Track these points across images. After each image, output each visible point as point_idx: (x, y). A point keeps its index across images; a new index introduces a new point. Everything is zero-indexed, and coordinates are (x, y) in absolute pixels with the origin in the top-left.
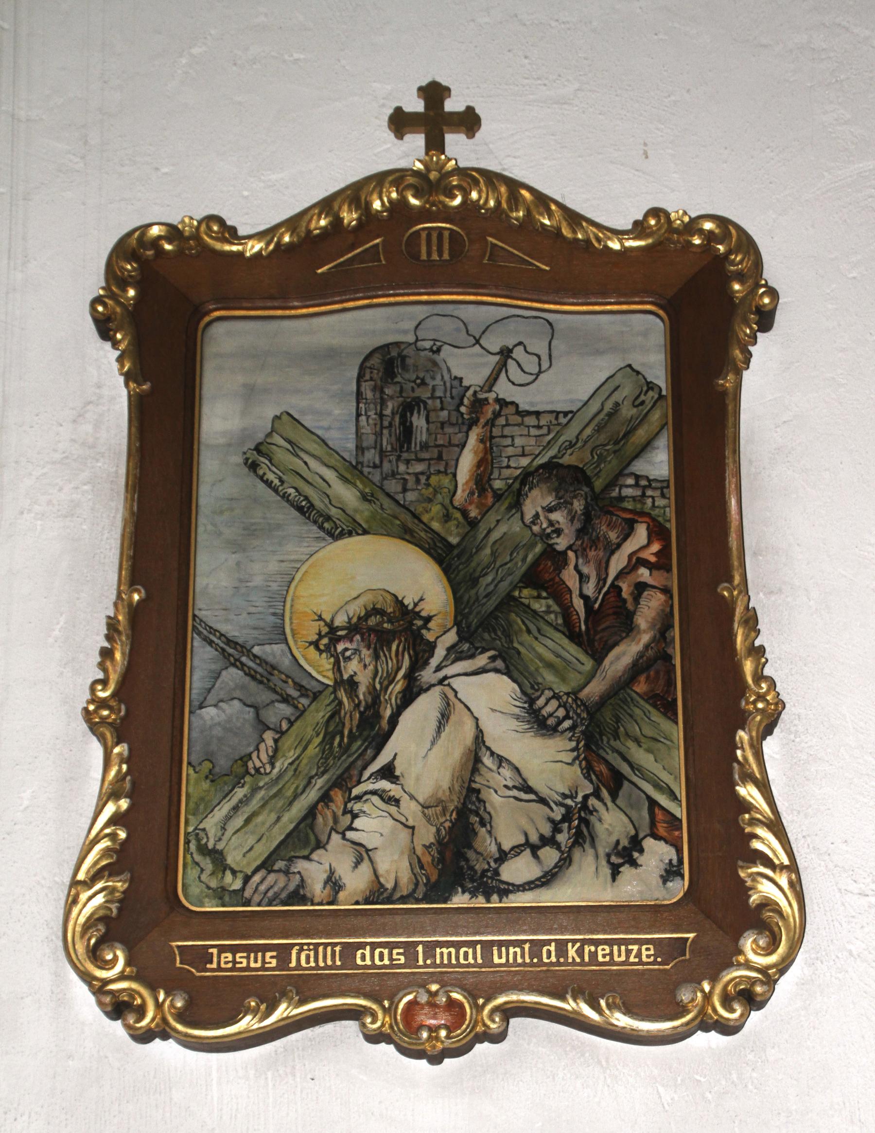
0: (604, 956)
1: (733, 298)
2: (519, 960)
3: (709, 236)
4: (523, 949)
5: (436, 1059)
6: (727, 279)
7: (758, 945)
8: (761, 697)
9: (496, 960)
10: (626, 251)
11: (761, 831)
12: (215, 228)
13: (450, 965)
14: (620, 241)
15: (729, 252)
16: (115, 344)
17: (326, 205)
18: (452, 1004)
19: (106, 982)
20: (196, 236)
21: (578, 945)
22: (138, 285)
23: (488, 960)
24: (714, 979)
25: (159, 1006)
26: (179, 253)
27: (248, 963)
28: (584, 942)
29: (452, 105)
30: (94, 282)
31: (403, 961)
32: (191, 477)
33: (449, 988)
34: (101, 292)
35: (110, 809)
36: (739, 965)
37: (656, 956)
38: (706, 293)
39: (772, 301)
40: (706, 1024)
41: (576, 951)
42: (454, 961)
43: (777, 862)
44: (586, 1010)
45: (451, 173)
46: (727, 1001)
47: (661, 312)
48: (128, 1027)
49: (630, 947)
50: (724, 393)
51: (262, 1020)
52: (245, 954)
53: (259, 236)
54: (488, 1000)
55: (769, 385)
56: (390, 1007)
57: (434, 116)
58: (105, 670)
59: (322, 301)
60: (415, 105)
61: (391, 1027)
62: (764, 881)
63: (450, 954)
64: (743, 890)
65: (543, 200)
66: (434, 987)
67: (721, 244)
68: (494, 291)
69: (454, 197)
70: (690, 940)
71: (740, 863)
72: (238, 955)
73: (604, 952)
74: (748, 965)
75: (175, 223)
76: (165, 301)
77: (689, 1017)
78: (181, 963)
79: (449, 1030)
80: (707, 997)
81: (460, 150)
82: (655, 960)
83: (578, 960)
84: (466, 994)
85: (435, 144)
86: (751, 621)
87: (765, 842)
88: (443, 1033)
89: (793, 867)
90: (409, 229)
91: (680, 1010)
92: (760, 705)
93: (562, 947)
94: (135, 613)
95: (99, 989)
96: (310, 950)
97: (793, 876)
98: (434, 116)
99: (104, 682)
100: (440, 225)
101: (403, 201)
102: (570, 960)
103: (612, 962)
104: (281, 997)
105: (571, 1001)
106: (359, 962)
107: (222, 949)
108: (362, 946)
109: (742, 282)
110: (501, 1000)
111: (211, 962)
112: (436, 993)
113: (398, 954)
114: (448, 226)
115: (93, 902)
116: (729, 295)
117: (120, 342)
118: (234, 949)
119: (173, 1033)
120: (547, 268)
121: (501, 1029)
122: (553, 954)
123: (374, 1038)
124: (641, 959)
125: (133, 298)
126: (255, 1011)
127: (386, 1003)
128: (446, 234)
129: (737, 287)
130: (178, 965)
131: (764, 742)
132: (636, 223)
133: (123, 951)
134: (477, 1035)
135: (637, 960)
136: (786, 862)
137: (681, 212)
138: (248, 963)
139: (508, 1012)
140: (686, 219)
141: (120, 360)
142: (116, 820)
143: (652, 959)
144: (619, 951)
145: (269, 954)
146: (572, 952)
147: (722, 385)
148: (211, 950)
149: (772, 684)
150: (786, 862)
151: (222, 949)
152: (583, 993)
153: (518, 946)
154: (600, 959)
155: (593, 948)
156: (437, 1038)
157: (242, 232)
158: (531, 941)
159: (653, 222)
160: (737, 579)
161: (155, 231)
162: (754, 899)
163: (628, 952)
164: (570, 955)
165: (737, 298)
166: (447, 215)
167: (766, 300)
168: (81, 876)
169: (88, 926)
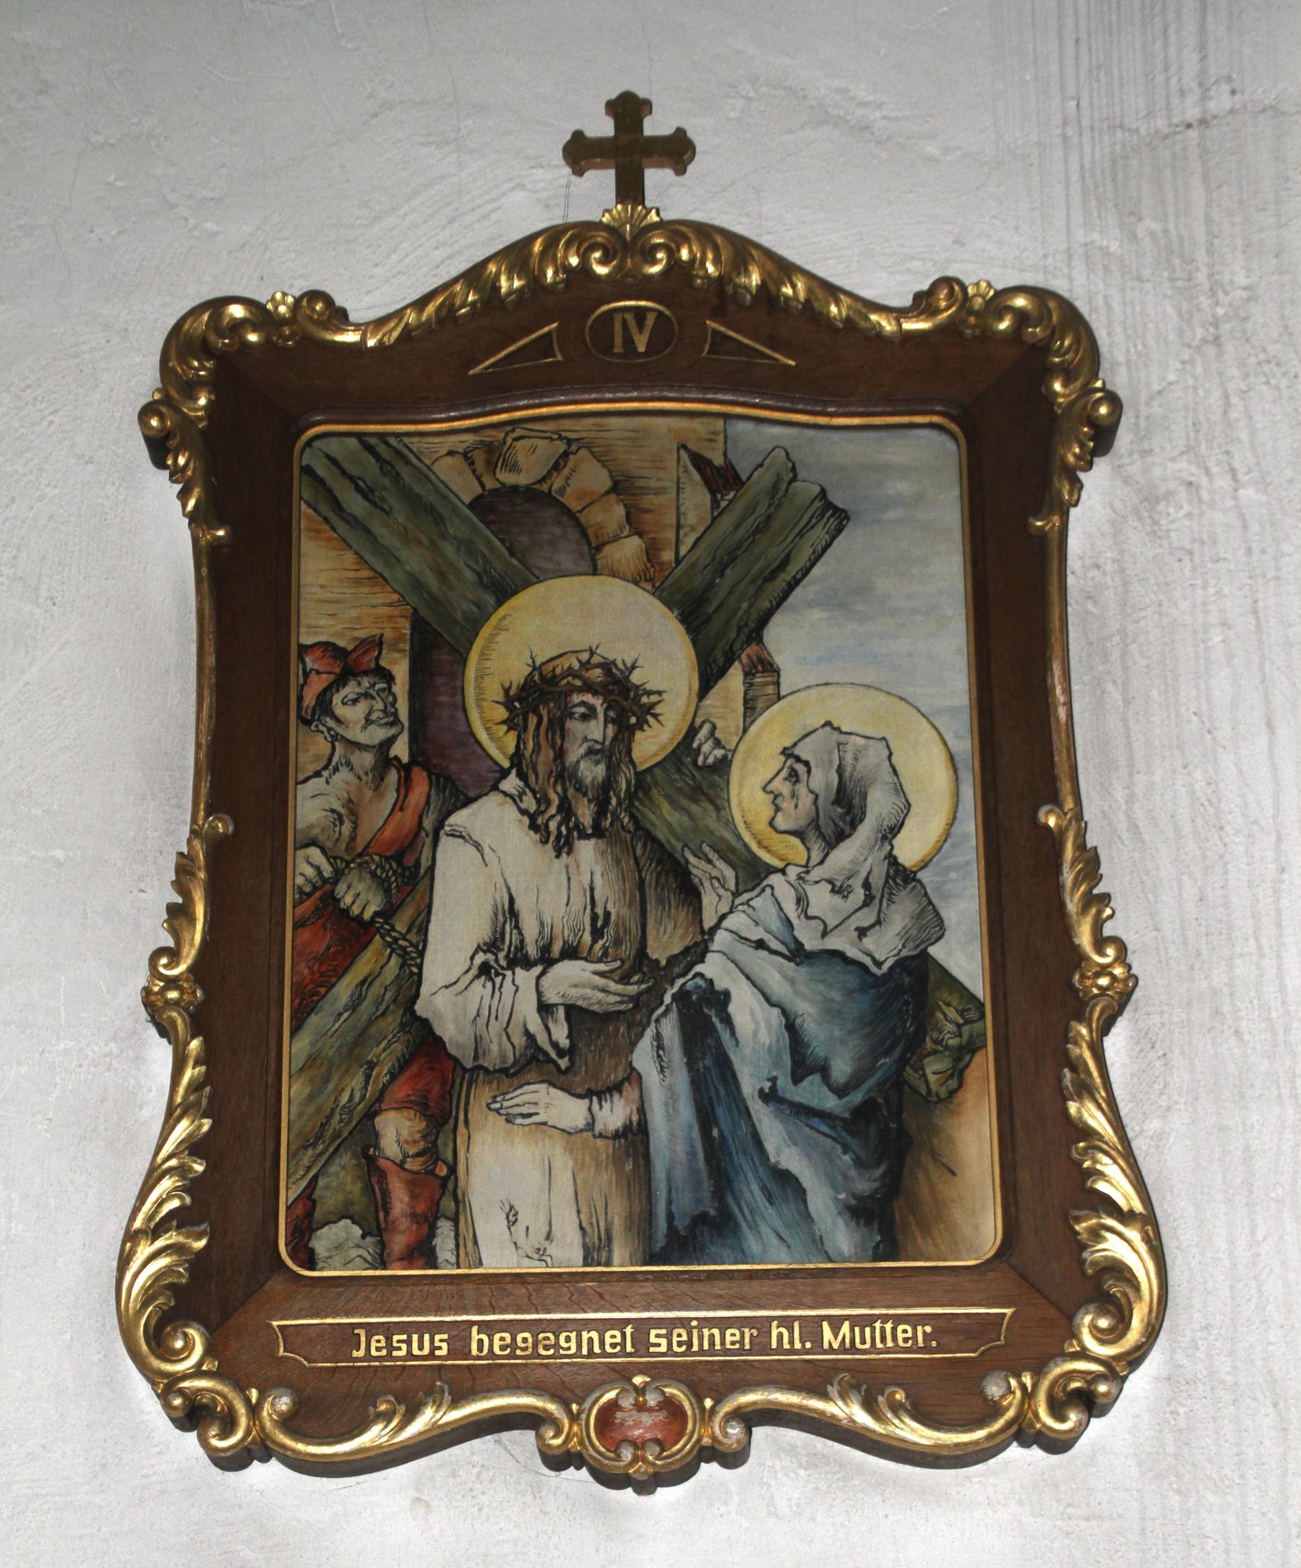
0: (503, 1348)
2: (879, 1345)
3: (1022, 317)
5: (645, 1486)
6: (1048, 372)
8: (1104, 970)
11: (1108, 1166)
17: (474, 276)
18: (670, 1406)
19: (177, 1378)
20: (292, 320)
22: (215, 384)
23: (642, 1344)
25: (254, 1410)
26: (267, 343)
27: (670, 1345)
29: (655, 126)
30: (144, 380)
34: (157, 396)
35: (183, 1129)
38: (1011, 401)
39: (1110, 414)
40: (1025, 1433)
42: (786, 1346)
44: (862, 1418)
45: (654, 226)
47: (953, 427)
48: (540, 1437)
50: (1042, 536)
52: (404, 1337)
53: (380, 323)
54: (717, 1402)
56: (579, 1413)
57: (630, 145)
58: (175, 933)
59: (478, 410)
60: (603, 127)
61: (581, 1443)
62: (1108, 1235)
65: (786, 269)
69: (654, 262)
72: (396, 1338)
74: (1084, 1354)
76: (253, 415)
77: (1000, 1423)
80: (1028, 1396)
81: (669, 196)
85: (630, 190)
86: (1091, 864)
89: (1148, 1222)
90: (609, 302)
91: (995, 1410)
92: (1104, 981)
95: (166, 1387)
97: (1149, 1228)
98: (630, 145)
99: (174, 955)
100: (643, 303)
101: (585, 268)
102: (826, 1346)
105: (840, 1403)
112: (640, 1391)
113: (441, 1341)
115: (150, 1264)
118: (388, 1330)
123: (557, 1461)
127: (574, 1407)
128: (650, 320)
129: (1057, 386)
132: (918, 297)
133: (202, 1335)
134: (703, 1449)
136: (1138, 1207)
140: (992, 293)
141: (183, 496)
142: (194, 1147)
150: (1138, 1207)
151: (371, 1329)
153: (683, 1327)
157: (353, 317)
160: (1069, 804)
161: (237, 311)
165: (1060, 405)
166: (645, 287)
168: (138, 1224)
169: (148, 1296)
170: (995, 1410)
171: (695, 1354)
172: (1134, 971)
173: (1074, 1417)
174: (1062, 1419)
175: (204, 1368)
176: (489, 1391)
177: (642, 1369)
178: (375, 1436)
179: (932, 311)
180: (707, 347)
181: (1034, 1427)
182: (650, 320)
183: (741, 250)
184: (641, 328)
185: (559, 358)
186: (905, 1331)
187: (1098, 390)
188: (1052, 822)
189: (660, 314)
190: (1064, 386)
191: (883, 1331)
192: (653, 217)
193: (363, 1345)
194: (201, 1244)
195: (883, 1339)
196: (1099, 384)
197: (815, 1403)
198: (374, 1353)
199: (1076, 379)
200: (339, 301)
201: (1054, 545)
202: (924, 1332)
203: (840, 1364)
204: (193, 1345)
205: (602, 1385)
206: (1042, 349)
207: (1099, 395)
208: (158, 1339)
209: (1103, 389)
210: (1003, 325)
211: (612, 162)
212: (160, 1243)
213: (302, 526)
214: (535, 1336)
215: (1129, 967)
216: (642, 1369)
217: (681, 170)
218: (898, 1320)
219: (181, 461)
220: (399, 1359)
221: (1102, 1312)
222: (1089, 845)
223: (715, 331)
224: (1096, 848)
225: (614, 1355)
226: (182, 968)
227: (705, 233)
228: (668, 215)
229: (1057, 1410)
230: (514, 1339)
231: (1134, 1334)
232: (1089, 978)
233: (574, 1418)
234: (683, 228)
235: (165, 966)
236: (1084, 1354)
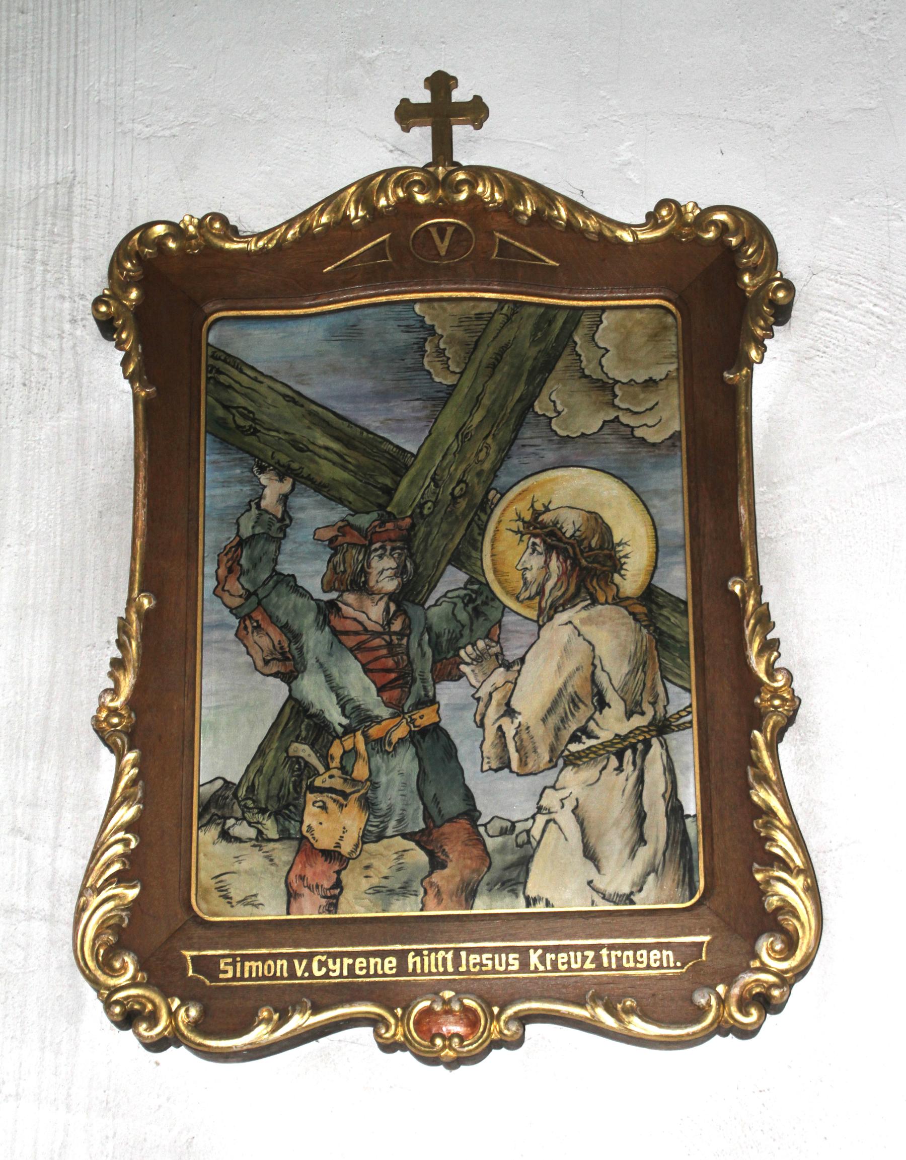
3: (723, 228)
5: (452, 1064)
7: (774, 951)
10: (637, 243)
13: (376, 975)
14: (634, 233)
15: (743, 243)
16: (119, 345)
17: (333, 201)
18: (466, 1010)
21: (540, 951)
25: (172, 1015)
28: (546, 949)
29: (459, 95)
30: (93, 278)
32: (198, 477)
33: (462, 996)
34: (106, 292)
35: (126, 814)
38: (719, 287)
40: (723, 1028)
43: (792, 865)
46: (743, 1005)
48: (138, 1035)
51: (273, 1031)
52: (490, 956)
53: (260, 236)
55: (775, 379)
56: (403, 1015)
57: (442, 109)
60: (423, 96)
61: (405, 1036)
63: (257, 967)
64: (760, 892)
65: (547, 196)
66: (448, 994)
67: (733, 237)
68: (434, 287)
70: (387, 244)
73: (391, 965)
74: (764, 969)
75: (177, 222)
76: (171, 298)
78: (193, 972)
79: (462, 1039)
81: (471, 147)
83: (541, 968)
84: (479, 1001)
85: (443, 146)
86: (765, 620)
87: (782, 843)
89: (808, 870)
91: (700, 1013)
94: (146, 617)
98: (442, 109)
99: (115, 692)
101: (410, 199)
102: (532, 968)
107: (470, 951)
109: (753, 274)
112: (446, 1002)
114: (460, 222)
117: (125, 341)
119: (184, 1041)
120: (552, 263)
123: (388, 1047)
124: (311, 972)
126: (268, 1021)
128: (450, 230)
129: (746, 278)
130: (190, 973)
131: (780, 746)
132: (649, 216)
135: (593, 966)
138: (494, 965)
139: (524, 1019)
141: (124, 363)
142: (129, 827)
143: (394, 971)
144: (576, 957)
145: (511, 956)
146: (534, 958)
150: (799, 861)
152: (602, 999)
154: (561, 967)
155: (619, 953)
159: (664, 212)
160: (750, 573)
161: (160, 230)
162: (773, 902)
163: (585, 958)
170: (700, 1013)
171: (246, 980)
174: (747, 1014)
176: (350, 1001)
177: (448, 985)
179: (656, 226)
182: (450, 230)
183: (516, 186)
184: (442, 239)
185: (390, 260)
186: (390, 962)
188: (737, 589)
190: (751, 279)
191: (444, 959)
195: (437, 966)
196: (778, 275)
200: (233, 221)
201: (742, 389)
205: (422, 996)
207: (776, 283)
208: (106, 966)
209: (781, 278)
211: (429, 120)
212: (104, 894)
214: (648, 953)
216: (448, 985)
217: (479, 127)
219: (124, 336)
220: (487, 972)
222: (763, 602)
223: (501, 240)
224: (768, 604)
229: (743, 1007)
231: (799, 955)
235: (112, 700)
236: (764, 969)
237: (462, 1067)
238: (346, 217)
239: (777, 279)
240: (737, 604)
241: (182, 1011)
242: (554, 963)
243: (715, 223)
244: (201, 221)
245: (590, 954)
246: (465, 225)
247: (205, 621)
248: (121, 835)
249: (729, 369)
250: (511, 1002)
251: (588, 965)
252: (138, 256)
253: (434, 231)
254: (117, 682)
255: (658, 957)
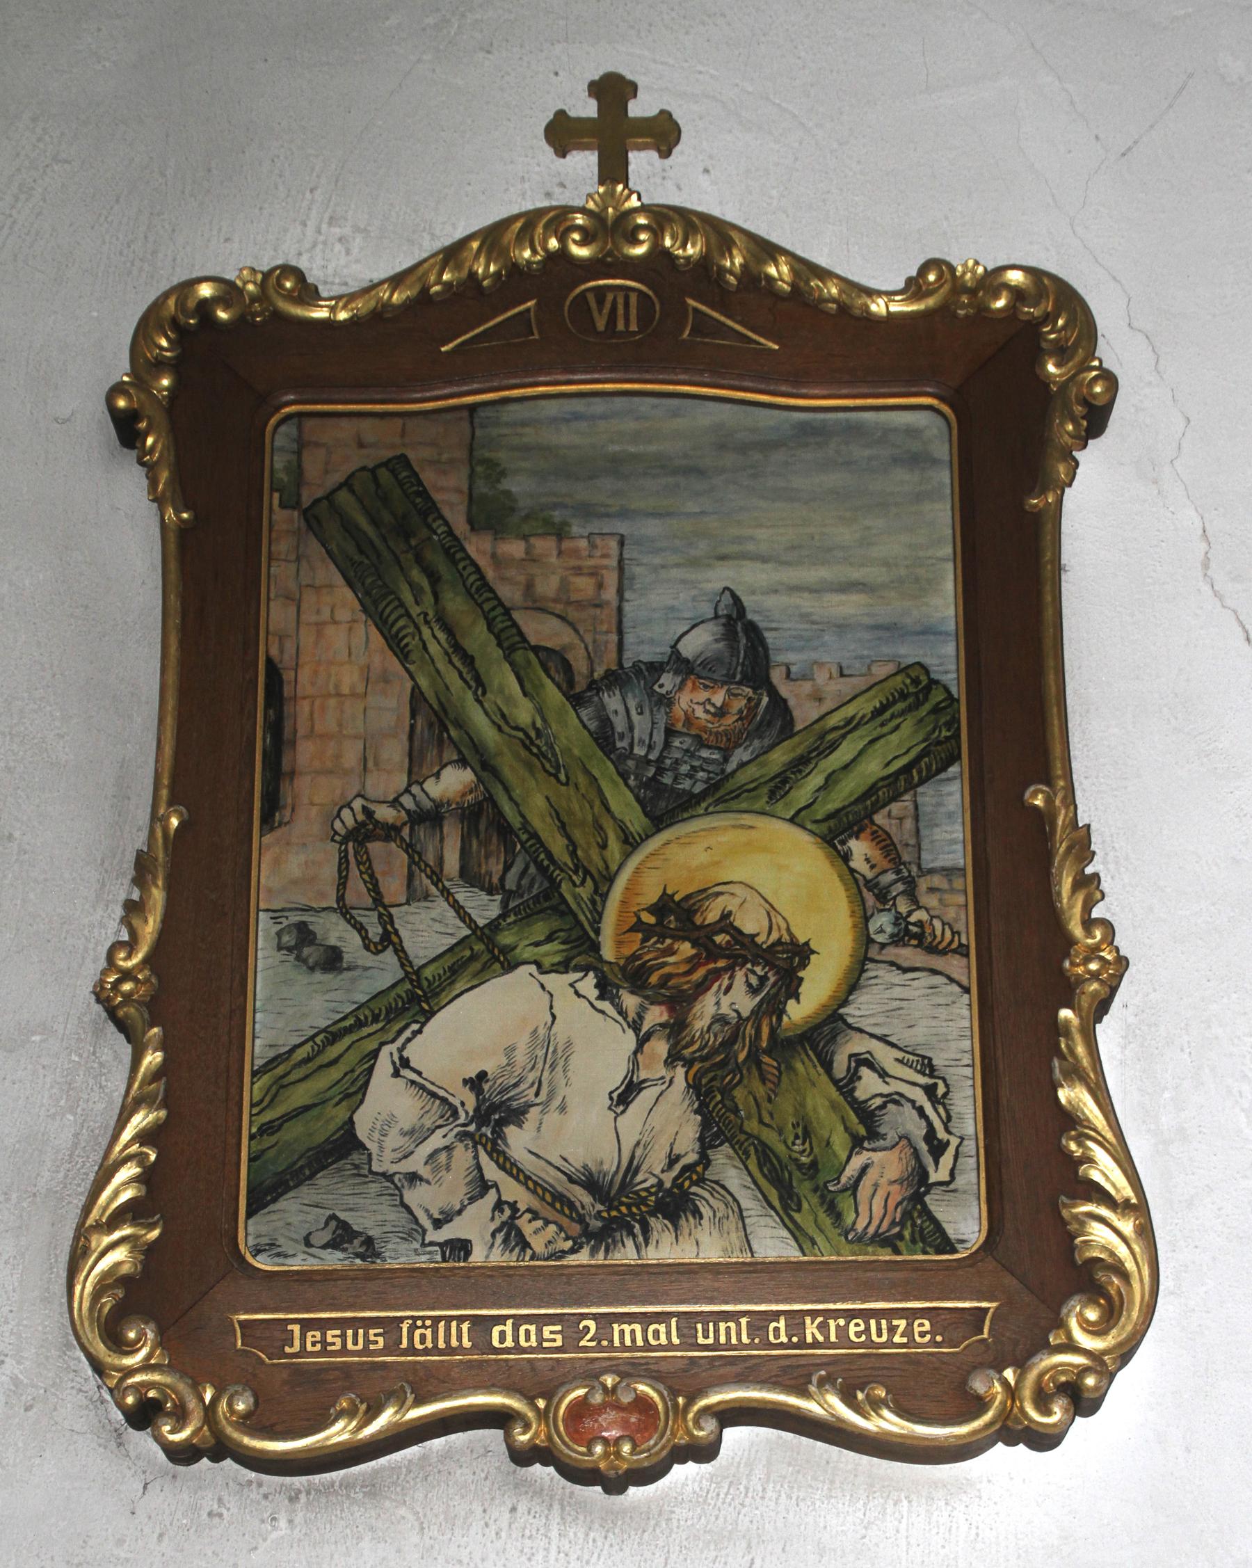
1: (1048, 385)
3: (1018, 294)
4: (739, 1325)
5: (615, 1485)
6: (1036, 355)
9: (701, 1340)
12: (288, 285)
19: (131, 1372)
21: (820, 1319)
24: (1021, 1365)
26: (241, 322)
29: (638, 109)
31: (559, 1343)
34: (126, 379)
35: (140, 1120)
36: (1061, 1349)
37: (933, 1332)
38: (1005, 384)
40: (1014, 1431)
41: (819, 1327)
42: (734, 1341)
43: (1117, 1197)
45: (635, 210)
47: (945, 408)
48: (159, 1439)
49: (895, 1322)
52: (338, 1332)
54: (691, 1401)
55: (1101, 508)
56: (547, 1407)
57: (613, 125)
58: (133, 933)
60: (587, 108)
63: (633, 1332)
64: (1067, 1237)
65: (768, 250)
71: (1063, 1198)
73: (858, 1329)
74: (1071, 1347)
76: (221, 393)
81: (651, 179)
82: (933, 1338)
85: (613, 171)
86: (1082, 847)
87: (1104, 1170)
88: (626, 1448)
89: (1139, 1208)
91: (978, 1405)
93: (795, 1321)
96: (424, 1327)
101: (563, 253)
102: (809, 1339)
103: (344, 1351)
104: (388, 1399)
106: (496, 1343)
107: (306, 1325)
108: (501, 1320)
110: (714, 1398)
111: (292, 1346)
116: (1043, 382)
120: (777, 347)
121: (712, 1437)
122: (700, 1334)
123: (521, 1457)
125: (166, 389)
126: (351, 1413)
127: (541, 1403)
129: (1051, 368)
131: (1097, 1026)
132: (910, 281)
137: (971, 263)
140: (980, 270)
142: (143, 1137)
143: (928, 1337)
144: (355, 1336)
146: (811, 1330)
147: (1036, 506)
148: (290, 1327)
149: (1108, 927)
150: (1128, 1192)
151: (306, 1325)
155: (842, 1322)
156: (618, 1454)
157: (324, 294)
158: (679, 1315)
159: (932, 277)
161: (206, 291)
163: (892, 1330)
164: (808, 1332)
167: (1098, 389)
170: (978, 1405)
172: (1122, 953)
173: (1057, 1414)
174: (1048, 1413)
175: (153, 1362)
178: (338, 1433)
180: (687, 332)
181: (1022, 1423)
183: (720, 232)
185: (536, 337)
187: (1094, 368)
189: (640, 292)
190: (1057, 365)
192: (634, 202)
193: (297, 1343)
194: (155, 1233)
196: (1096, 363)
197: (793, 1400)
198: (309, 1348)
199: (1071, 358)
202: (838, 1326)
203: (945, 1359)
204: (141, 1354)
206: (1033, 328)
207: (1094, 373)
209: (1100, 368)
210: (1000, 303)
213: (260, 946)
215: (1117, 950)
217: (666, 153)
218: (850, 1315)
219: (150, 441)
221: (1093, 1301)
222: (1080, 825)
223: (695, 310)
224: (1088, 826)
225: (860, 1345)
226: (135, 960)
227: (689, 221)
228: (646, 200)
229: (1042, 1402)
230: (324, 1335)
232: (1078, 965)
233: (543, 1415)
234: (665, 211)
236: (1071, 1347)
237: (1021, 1447)
238: (472, 275)
239: (1094, 368)
240: (1041, 822)
241: (223, 1405)
242: (843, 1331)
243: (1006, 286)
244: (267, 275)
245: (902, 1324)
246: (651, 293)
247: (954, 643)
248: (135, 1148)
249: (1030, 492)
250: (701, 1392)
251: (897, 1339)
252: (174, 323)
253: (591, 298)
254: (133, 933)
255: (862, 1328)
